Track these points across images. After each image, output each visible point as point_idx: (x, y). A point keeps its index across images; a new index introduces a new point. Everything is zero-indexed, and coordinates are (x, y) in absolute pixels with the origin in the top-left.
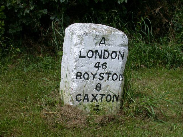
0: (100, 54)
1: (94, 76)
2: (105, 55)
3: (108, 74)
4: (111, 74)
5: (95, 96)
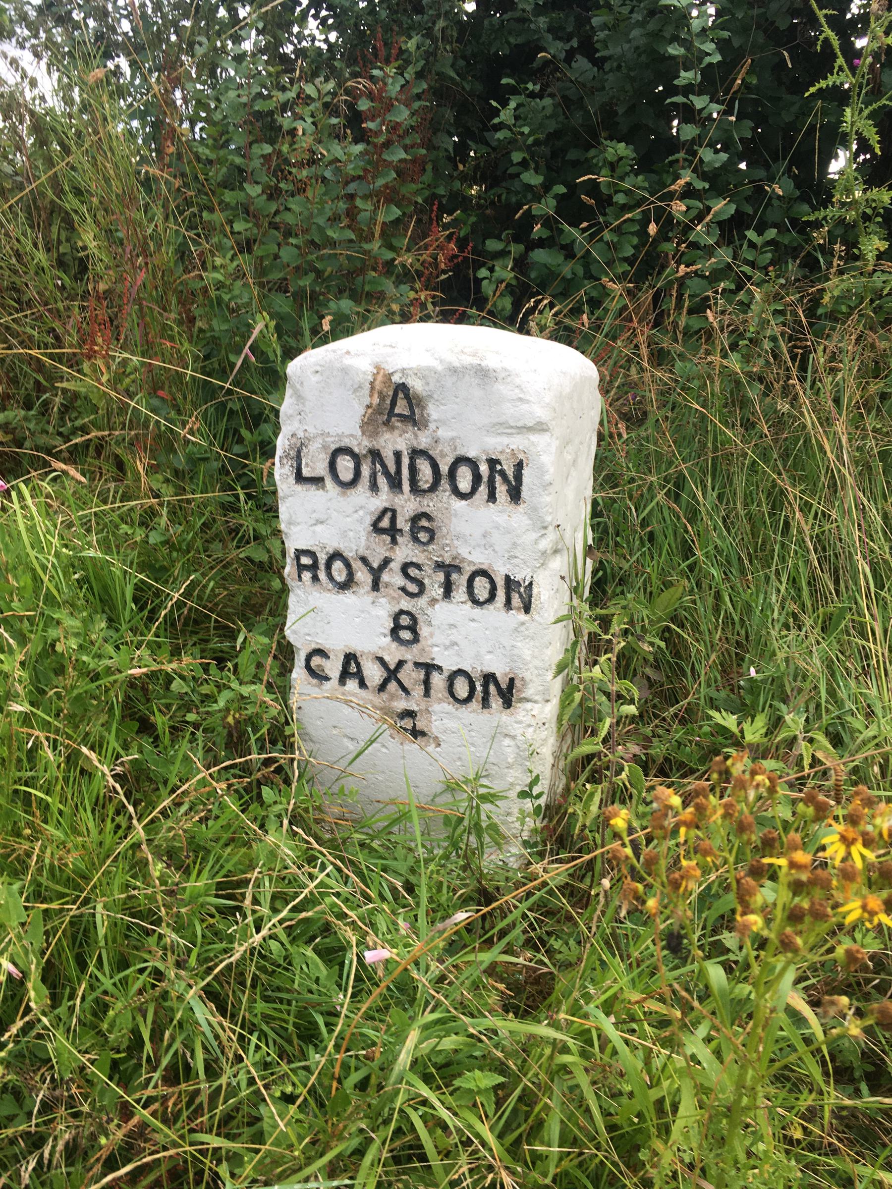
0: (392, 469)
1: (376, 574)
2: (420, 476)
3: (448, 569)
4: (458, 569)
5: (392, 667)
